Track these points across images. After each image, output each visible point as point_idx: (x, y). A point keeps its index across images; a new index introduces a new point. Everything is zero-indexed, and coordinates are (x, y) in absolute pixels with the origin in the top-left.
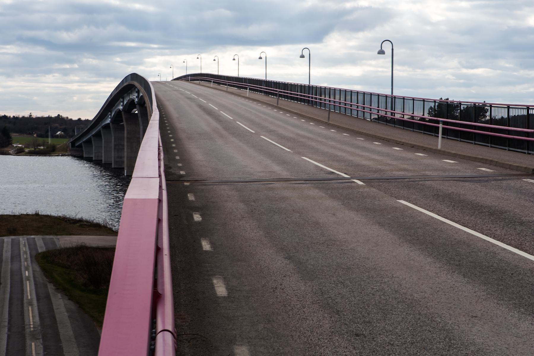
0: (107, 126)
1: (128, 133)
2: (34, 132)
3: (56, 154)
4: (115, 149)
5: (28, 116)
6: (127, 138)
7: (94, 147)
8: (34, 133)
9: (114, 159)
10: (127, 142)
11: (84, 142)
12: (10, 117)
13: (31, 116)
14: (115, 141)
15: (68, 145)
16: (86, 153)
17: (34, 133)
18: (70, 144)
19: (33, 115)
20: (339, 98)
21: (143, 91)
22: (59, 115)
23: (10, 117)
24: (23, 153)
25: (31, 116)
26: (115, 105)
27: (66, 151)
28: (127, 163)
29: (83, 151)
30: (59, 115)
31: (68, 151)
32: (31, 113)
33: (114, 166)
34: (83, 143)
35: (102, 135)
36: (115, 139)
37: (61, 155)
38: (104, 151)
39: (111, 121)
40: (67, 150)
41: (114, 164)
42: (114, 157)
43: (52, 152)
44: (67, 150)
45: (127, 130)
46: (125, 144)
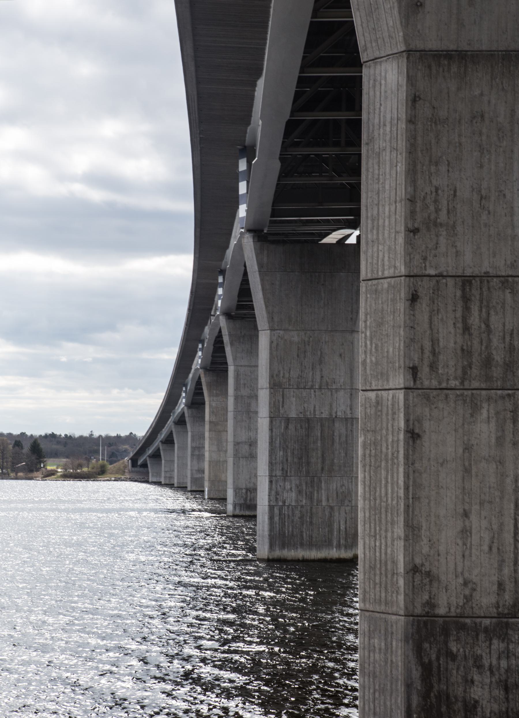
0: (181, 422)
1: (212, 413)
2: (93, 456)
3: (106, 478)
4: (192, 455)
5: (88, 436)
6: (210, 422)
7: (163, 462)
8: (92, 458)
9: (192, 474)
10: (210, 430)
11: (150, 456)
12: (60, 435)
13: (92, 435)
14: (193, 440)
15: (127, 464)
16: (153, 476)
17: (92, 458)
18: (130, 461)
19: (94, 434)
20: (338, 526)
21: (263, 531)
22: (131, 433)
23: (60, 435)
24: (53, 477)
25: (92, 435)
26: (191, 369)
27: (123, 473)
28: (210, 473)
29: (148, 473)
30: (131, 433)
31: (126, 474)
32: (92, 432)
33: (191, 487)
34: (148, 459)
35: (176, 441)
36: (193, 436)
37: (113, 479)
38: (178, 466)
39: (186, 405)
40: (124, 472)
41: (191, 483)
42: (191, 470)
43: (99, 474)
44: (124, 472)
45: (210, 406)
46: (207, 434)
